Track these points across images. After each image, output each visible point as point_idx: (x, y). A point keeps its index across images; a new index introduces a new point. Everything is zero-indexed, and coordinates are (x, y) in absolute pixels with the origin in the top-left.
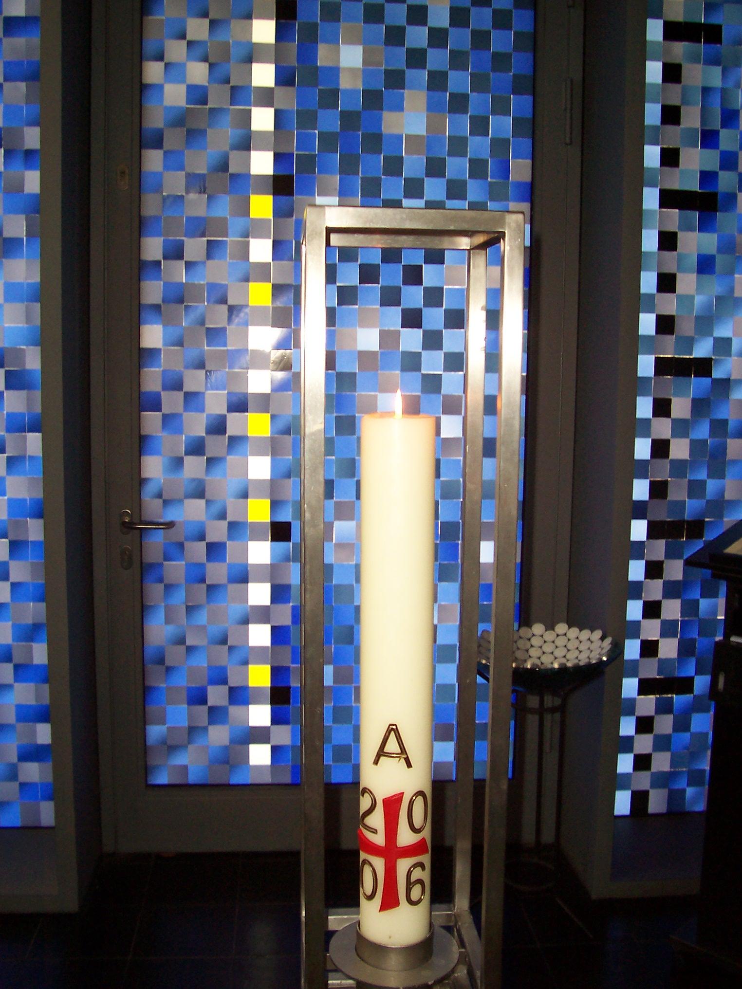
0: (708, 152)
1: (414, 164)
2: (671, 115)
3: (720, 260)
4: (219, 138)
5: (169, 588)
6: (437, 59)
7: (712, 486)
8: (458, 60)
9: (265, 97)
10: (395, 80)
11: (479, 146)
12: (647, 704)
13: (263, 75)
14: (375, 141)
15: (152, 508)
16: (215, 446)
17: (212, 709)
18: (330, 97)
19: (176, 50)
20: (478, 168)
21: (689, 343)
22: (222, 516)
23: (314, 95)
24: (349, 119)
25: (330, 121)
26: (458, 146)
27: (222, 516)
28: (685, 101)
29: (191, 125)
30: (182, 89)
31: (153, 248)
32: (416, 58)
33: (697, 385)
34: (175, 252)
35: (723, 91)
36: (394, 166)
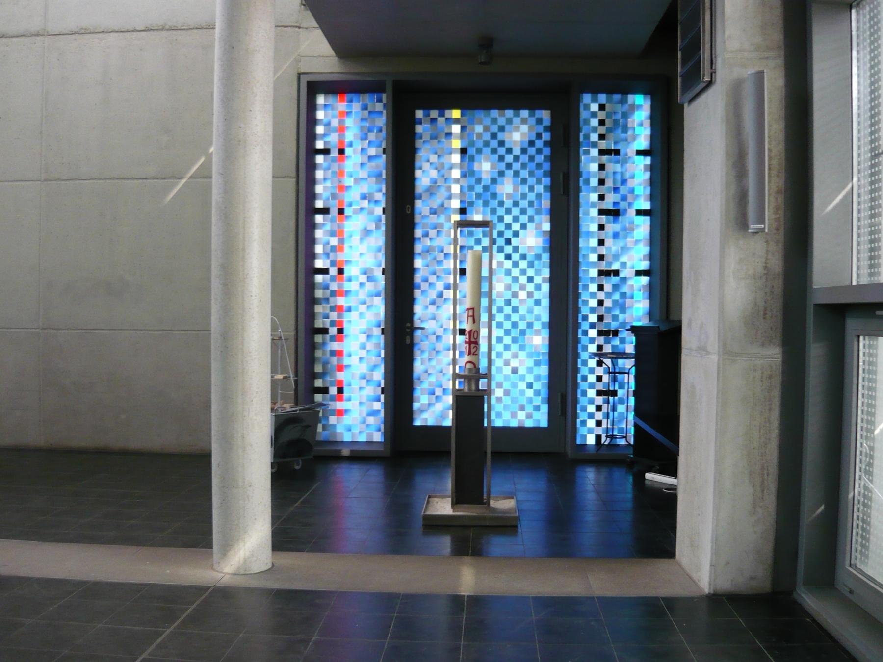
0: (616, 195)
1: (508, 203)
2: (602, 182)
3: (621, 234)
4: (442, 193)
5: (422, 351)
6: (516, 166)
7: (621, 317)
8: (524, 166)
9: (457, 181)
10: (501, 174)
11: (531, 196)
12: (600, 400)
13: (456, 173)
14: (494, 196)
15: (417, 323)
16: (439, 301)
17: (437, 397)
18: (479, 181)
19: (426, 166)
20: (531, 204)
21: (610, 264)
22: (442, 327)
23: (472, 181)
24: (486, 188)
25: (479, 189)
26: (524, 196)
27: (442, 327)
28: (607, 177)
29: (431, 191)
30: (428, 179)
31: (418, 233)
32: (509, 166)
33: (615, 279)
34: (426, 235)
35: (622, 173)
36: (501, 204)
